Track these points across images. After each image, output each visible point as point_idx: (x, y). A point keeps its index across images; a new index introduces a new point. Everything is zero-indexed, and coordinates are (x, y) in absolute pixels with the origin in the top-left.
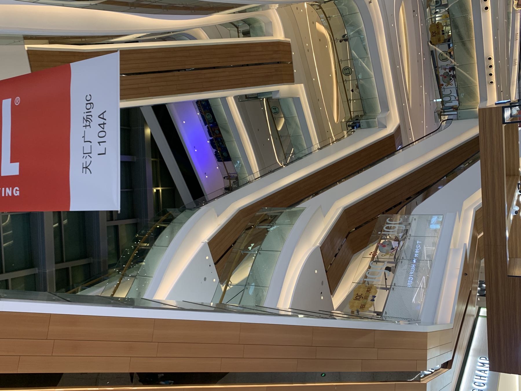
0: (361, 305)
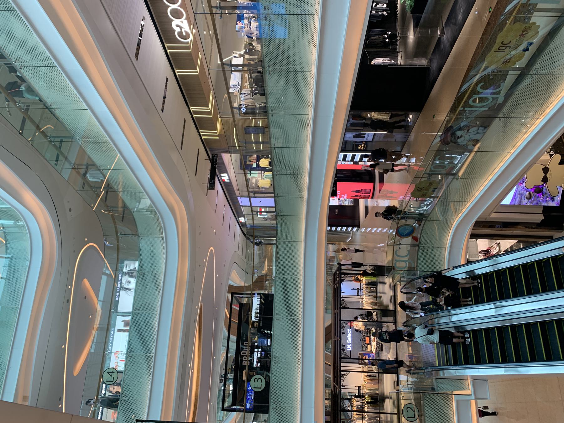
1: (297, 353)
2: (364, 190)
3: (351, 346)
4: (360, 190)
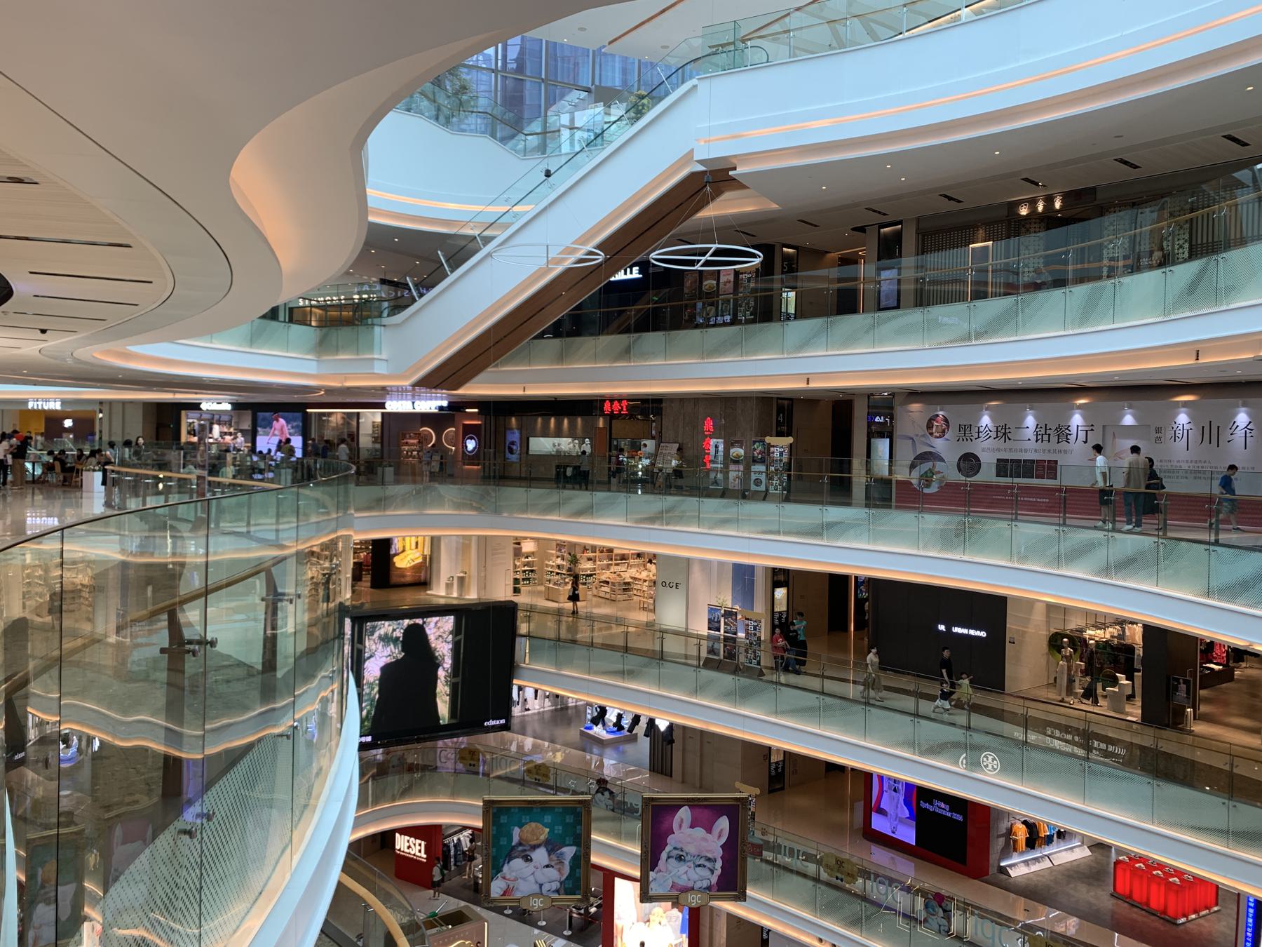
1: (891, 746)
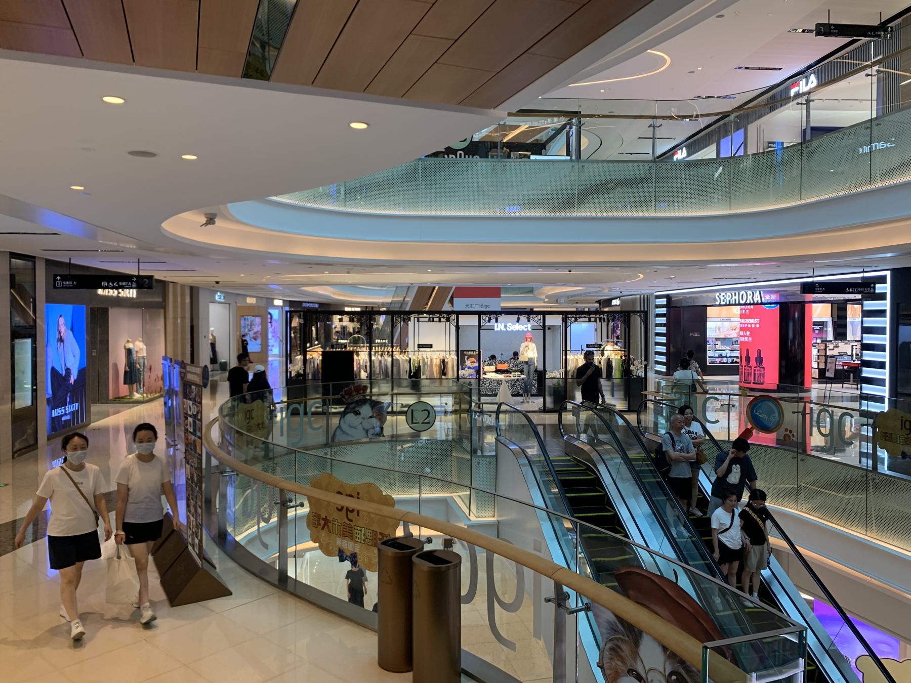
0: (891, 434)
2: (762, 372)
3: (503, 329)
4: (763, 365)
